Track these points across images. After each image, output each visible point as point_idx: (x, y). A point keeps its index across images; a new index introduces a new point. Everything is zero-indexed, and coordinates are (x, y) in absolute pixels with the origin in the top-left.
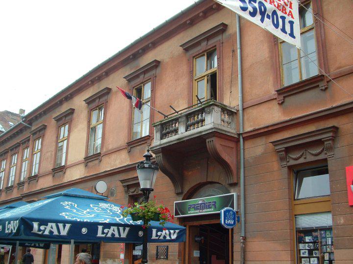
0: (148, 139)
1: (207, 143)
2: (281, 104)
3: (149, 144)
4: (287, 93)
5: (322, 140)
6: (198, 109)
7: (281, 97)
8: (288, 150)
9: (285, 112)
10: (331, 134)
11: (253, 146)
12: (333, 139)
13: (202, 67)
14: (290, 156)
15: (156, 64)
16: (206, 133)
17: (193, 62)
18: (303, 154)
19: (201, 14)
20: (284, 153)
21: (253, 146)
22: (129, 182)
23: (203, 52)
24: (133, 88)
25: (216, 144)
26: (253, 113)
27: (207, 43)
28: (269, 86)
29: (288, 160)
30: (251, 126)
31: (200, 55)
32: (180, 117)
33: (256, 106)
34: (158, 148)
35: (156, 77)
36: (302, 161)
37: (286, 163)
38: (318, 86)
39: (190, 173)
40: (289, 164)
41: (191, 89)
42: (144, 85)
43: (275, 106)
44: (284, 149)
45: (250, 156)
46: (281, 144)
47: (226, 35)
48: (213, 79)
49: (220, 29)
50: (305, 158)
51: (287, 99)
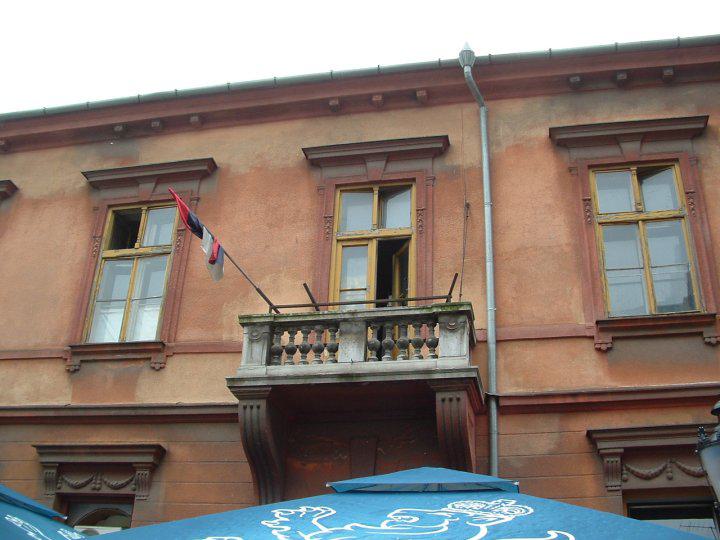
0: (159, 351)
1: (439, 404)
2: (72, 372)
3: (157, 366)
4: (618, 332)
5: (134, 465)
6: (417, 312)
7: (607, 338)
8: (629, 455)
9: (613, 370)
10: (150, 459)
11: (523, 431)
12: (154, 468)
13: (358, 216)
14: (66, 479)
15: (207, 169)
16: (448, 376)
17: (106, 216)
18: (664, 469)
19: (377, 98)
20: (618, 459)
21: (523, 431)
22: (72, 454)
23: (371, 183)
24: (110, 206)
25: (451, 407)
26: (529, 355)
27: (156, 187)
28: (571, 307)
29: (625, 476)
30: (518, 385)
31: (364, 188)
32: (345, 320)
33: (533, 343)
34: (260, 383)
35: (198, 199)
36: (660, 482)
37: (619, 483)
38: (150, 359)
39: (310, 466)
40: (626, 486)
41: (322, 264)
42: (149, 209)
43: (586, 354)
44: (622, 450)
45: (515, 453)
46: (104, 454)
47: (438, 166)
48: (391, 254)
49: (434, 146)
50: (670, 479)
51: (618, 345)
